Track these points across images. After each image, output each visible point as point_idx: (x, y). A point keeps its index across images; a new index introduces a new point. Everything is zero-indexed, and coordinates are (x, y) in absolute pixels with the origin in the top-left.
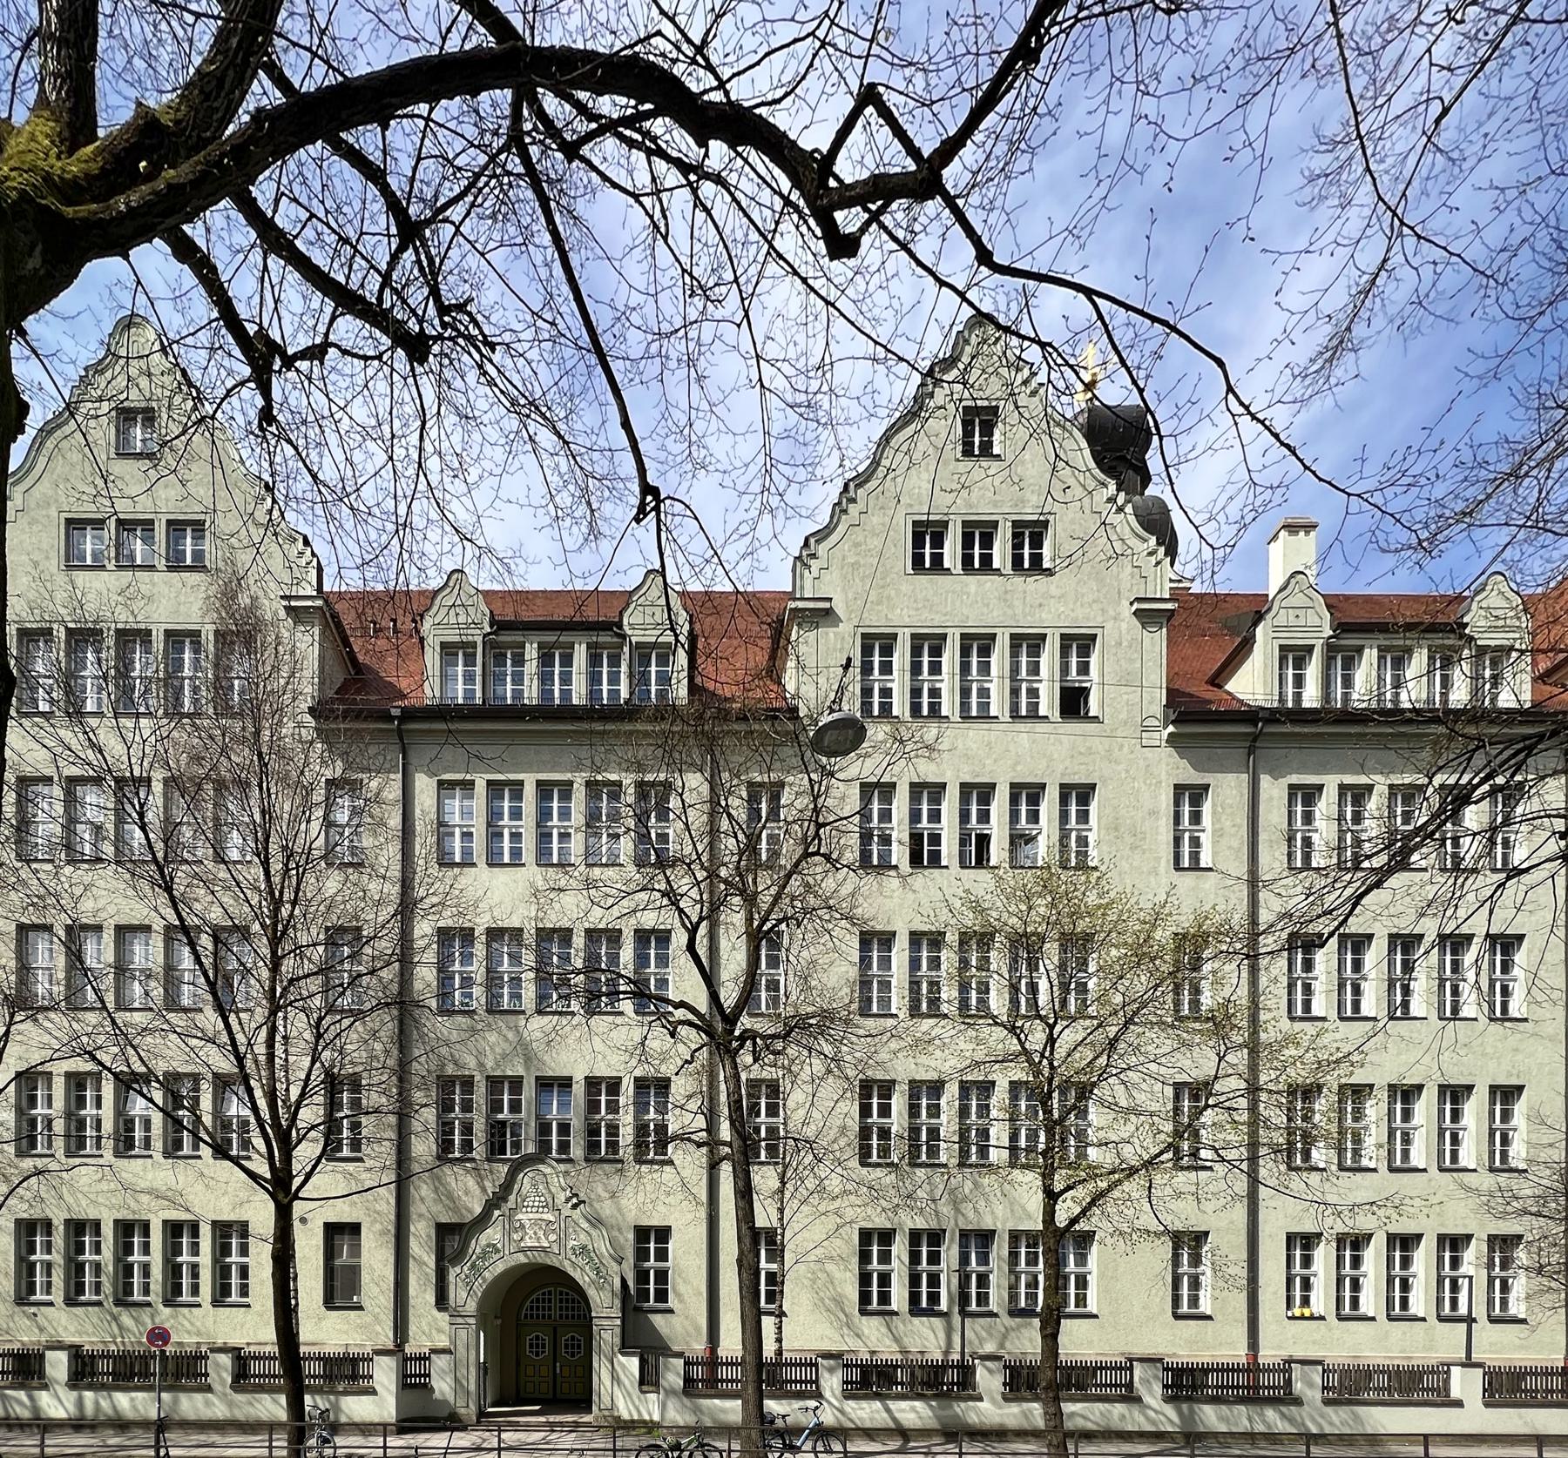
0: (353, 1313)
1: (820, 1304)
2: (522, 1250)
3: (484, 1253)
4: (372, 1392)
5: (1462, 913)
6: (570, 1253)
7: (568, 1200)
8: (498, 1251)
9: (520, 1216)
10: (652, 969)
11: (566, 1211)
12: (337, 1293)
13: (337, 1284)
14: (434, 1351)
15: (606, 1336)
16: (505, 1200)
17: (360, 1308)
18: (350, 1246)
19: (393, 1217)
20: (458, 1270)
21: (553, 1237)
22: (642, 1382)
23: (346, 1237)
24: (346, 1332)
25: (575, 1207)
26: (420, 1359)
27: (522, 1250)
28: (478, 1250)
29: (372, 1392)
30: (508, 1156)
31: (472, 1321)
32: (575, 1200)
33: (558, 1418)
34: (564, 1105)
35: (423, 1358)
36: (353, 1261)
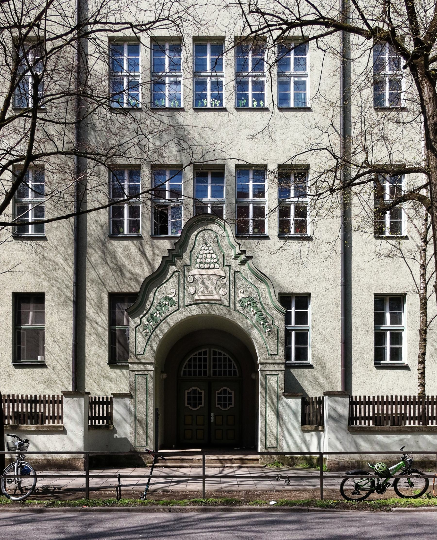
0: (38, 370)
1: (362, 29)
2: (197, 303)
3: (161, 305)
4: (62, 431)
5: (396, 18)
6: (238, 305)
7: (237, 257)
8: (173, 303)
9: (194, 272)
10: (209, 72)
11: (235, 264)
12: (24, 353)
13: (24, 346)
14: (116, 395)
15: (272, 380)
16: (179, 257)
17: (43, 366)
18: (35, 313)
19: (71, 285)
20: (137, 320)
21: (222, 292)
22: (304, 423)
23: (32, 305)
24: (33, 386)
25: (243, 262)
26: (103, 403)
27: (197, 303)
28: (155, 303)
29: (62, 431)
30: (170, 234)
31: (151, 367)
32: (243, 257)
33: (226, 457)
34: (217, 192)
35: (108, 402)
36: (37, 327)
